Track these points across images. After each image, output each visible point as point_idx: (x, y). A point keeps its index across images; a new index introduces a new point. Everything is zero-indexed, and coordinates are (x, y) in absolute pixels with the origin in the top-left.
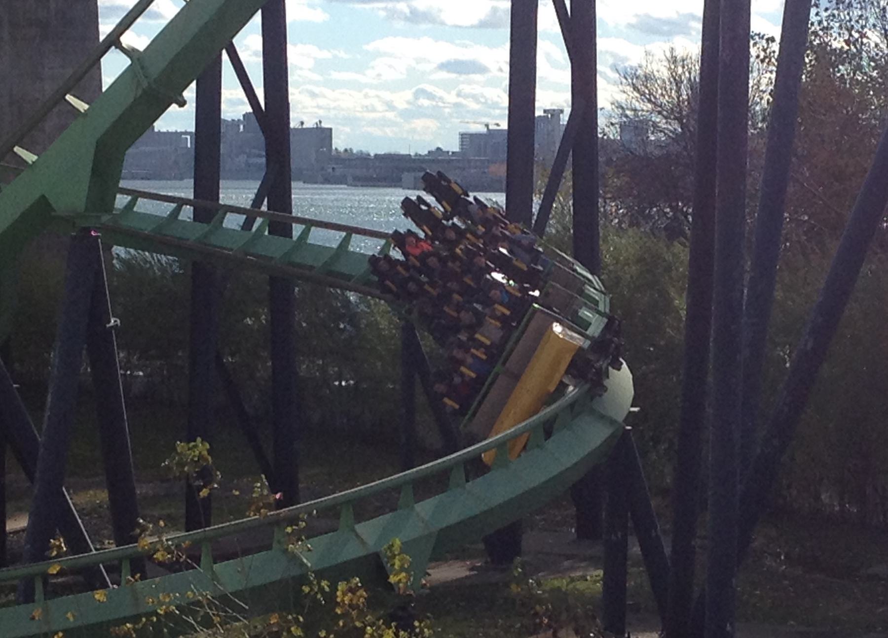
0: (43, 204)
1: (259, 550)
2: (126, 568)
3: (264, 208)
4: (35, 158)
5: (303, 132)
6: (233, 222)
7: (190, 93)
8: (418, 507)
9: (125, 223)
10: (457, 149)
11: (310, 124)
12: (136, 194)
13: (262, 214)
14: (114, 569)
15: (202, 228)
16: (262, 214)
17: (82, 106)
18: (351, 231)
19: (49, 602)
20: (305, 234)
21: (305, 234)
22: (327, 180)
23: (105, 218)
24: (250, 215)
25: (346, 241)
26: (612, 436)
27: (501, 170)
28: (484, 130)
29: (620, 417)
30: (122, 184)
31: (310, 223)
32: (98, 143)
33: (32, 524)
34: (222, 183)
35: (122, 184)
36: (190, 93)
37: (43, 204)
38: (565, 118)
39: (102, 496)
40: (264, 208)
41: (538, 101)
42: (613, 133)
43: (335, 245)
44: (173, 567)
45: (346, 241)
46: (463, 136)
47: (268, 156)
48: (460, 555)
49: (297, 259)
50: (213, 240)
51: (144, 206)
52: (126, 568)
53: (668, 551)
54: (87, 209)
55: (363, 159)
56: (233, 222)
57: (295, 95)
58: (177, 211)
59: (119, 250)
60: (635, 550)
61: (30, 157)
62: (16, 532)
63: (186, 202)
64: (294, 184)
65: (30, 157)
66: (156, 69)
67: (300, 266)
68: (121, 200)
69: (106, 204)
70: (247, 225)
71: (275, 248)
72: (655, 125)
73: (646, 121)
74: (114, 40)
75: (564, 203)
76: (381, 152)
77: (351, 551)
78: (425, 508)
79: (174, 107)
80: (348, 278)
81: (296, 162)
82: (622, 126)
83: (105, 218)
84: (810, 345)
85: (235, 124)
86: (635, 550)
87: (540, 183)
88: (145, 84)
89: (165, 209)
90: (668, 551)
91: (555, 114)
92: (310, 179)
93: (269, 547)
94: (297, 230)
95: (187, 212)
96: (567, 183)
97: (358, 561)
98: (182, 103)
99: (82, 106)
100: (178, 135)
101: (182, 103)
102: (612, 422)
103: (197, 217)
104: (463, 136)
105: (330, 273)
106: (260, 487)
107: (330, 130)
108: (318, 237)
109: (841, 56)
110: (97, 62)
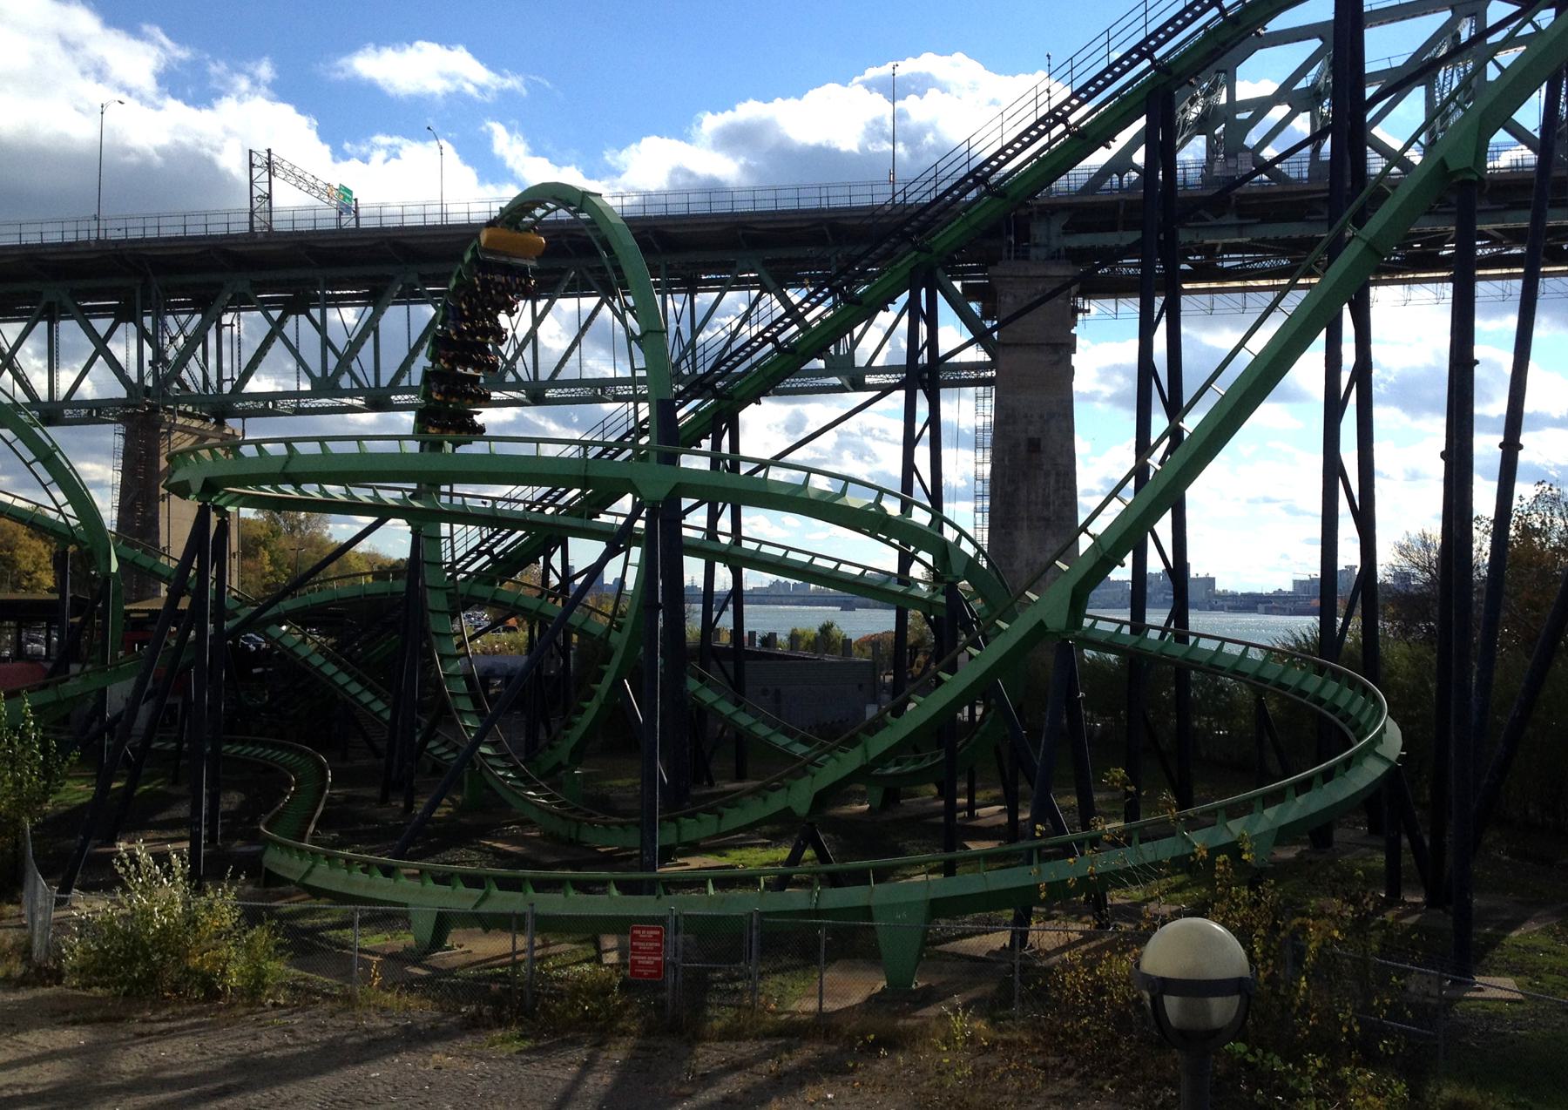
0: (1041, 624)
1: (1168, 836)
2: (1087, 845)
3: (1172, 626)
4: (1037, 598)
5: (1198, 580)
6: (1154, 635)
7: (1128, 559)
8: (1266, 812)
9: (1091, 635)
10: (1291, 590)
11: (1202, 575)
12: (1096, 619)
13: (1171, 630)
14: (1080, 844)
15: (1136, 638)
16: (1171, 630)
17: (1065, 567)
18: (1224, 640)
19: (1042, 865)
20: (1196, 642)
21: (1196, 642)
22: (1212, 609)
23: (1077, 633)
24: (1164, 630)
25: (1221, 647)
26: (1388, 771)
27: (1316, 602)
28: (1308, 578)
29: (1393, 757)
30: (1088, 612)
31: (1199, 636)
32: (679, 483)
33: (1031, 816)
34: (1148, 610)
35: (1088, 612)
36: (1128, 559)
37: (1041, 624)
38: (1357, 570)
39: (1074, 801)
40: (1172, 626)
41: (1309, 541)
42: (1390, 581)
43: (1114, 630)
44: (1115, 844)
45: (1221, 647)
46: (1295, 582)
47: (1174, 594)
48: (1296, 842)
49: (1140, 646)
50: (1143, 645)
51: (1101, 625)
52: (1087, 845)
53: (1427, 843)
54: (1067, 628)
55: (1234, 596)
56: (1154, 635)
57: (1191, 558)
58: (1120, 629)
59: (1088, 653)
60: (1405, 841)
61: (1034, 597)
62: (1024, 821)
63: (1125, 623)
64: (1190, 611)
65: (1034, 597)
66: (1107, 545)
67: (1192, 661)
68: (1087, 622)
69: (1079, 625)
70: (1162, 637)
71: (1178, 650)
72: (1414, 575)
73: (1408, 574)
74: (1084, 529)
75: (1356, 623)
76: (1245, 591)
77: (1225, 839)
78: (1270, 813)
79: (1118, 567)
80: (1223, 668)
81: (1191, 598)
82: (1395, 577)
83: (1077, 633)
84: (1518, 714)
85: (1157, 575)
86: (1405, 841)
87: (1341, 608)
88: (1101, 554)
89: (1113, 627)
90: (1427, 843)
91: (1352, 568)
92: (1201, 607)
93: (1173, 835)
94: (1192, 639)
95: (1126, 630)
96: (1358, 610)
97: (1227, 845)
98: (1123, 565)
99: (1065, 567)
100: (1123, 582)
101: (1123, 565)
102: (1389, 761)
103: (1132, 632)
104: (1295, 582)
105: (1211, 666)
106: (1167, 796)
107: (1214, 579)
108: (1204, 644)
109: (1538, 532)
110: (1077, 538)
